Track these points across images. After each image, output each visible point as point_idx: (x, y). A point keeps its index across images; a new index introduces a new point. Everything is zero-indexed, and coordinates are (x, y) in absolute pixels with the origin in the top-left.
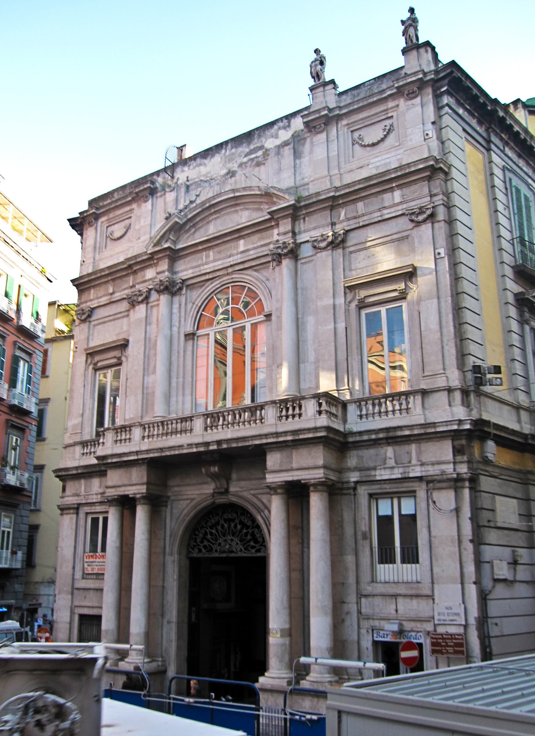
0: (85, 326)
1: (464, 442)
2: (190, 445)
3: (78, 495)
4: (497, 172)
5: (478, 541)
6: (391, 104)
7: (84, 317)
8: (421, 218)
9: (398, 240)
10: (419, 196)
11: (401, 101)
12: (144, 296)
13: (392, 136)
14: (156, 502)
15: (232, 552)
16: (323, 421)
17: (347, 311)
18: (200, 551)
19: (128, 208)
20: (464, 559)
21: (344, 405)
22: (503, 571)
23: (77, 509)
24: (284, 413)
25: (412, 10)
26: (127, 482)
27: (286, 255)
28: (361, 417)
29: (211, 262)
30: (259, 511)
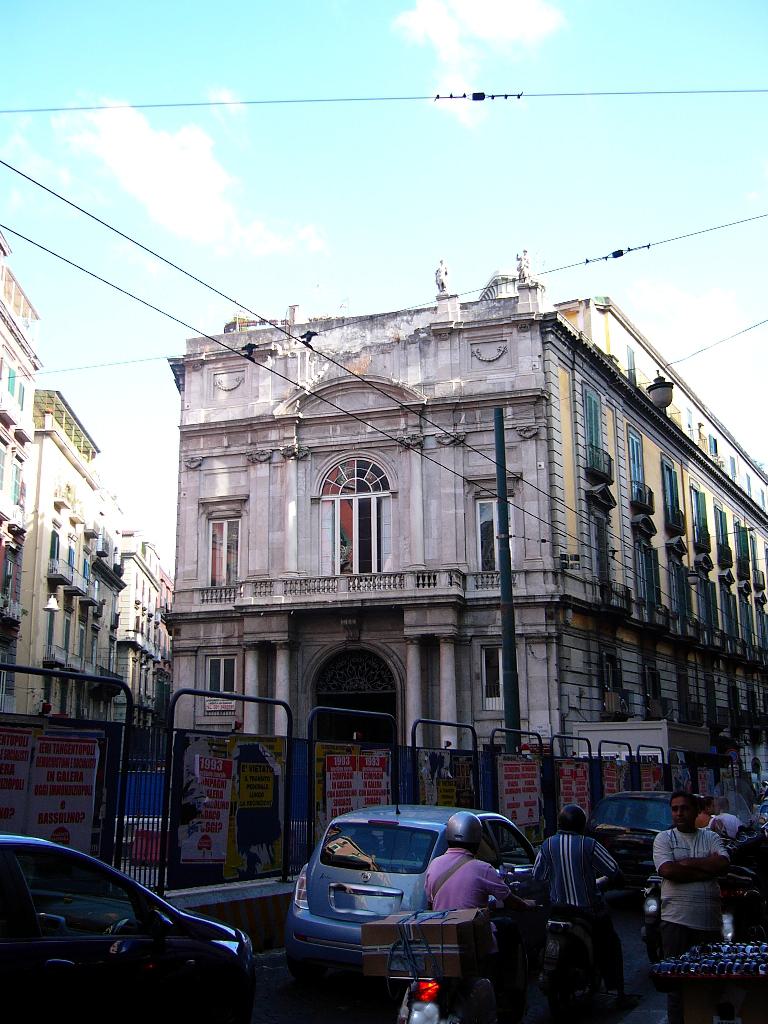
1: (553, 610)
2: (335, 602)
3: (196, 639)
4: (578, 388)
5: (561, 681)
6: (506, 330)
12: (267, 456)
14: (293, 647)
15: (360, 690)
16: (455, 590)
18: (329, 689)
20: (551, 693)
21: (464, 577)
22: (574, 703)
23: (196, 651)
24: (421, 581)
26: (266, 630)
27: (415, 445)
28: (477, 587)
30: (390, 657)
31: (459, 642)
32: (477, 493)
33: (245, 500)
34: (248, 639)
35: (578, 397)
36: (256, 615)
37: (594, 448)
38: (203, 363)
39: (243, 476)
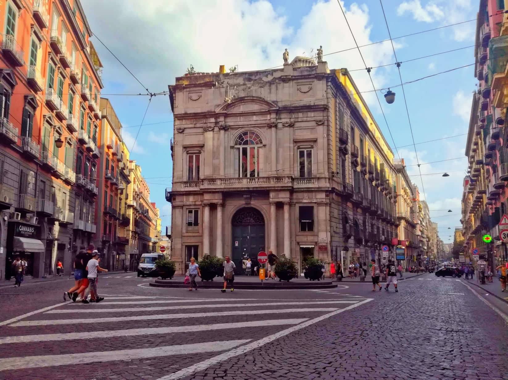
0: (181, 135)
3: (183, 202)
7: (181, 131)
8: (320, 123)
9: (312, 129)
10: (319, 116)
11: (315, 80)
13: (311, 91)
16: (290, 185)
17: (294, 149)
19: (200, 88)
25: (321, 47)
29: (241, 121)
31: (290, 204)
32: (298, 146)
33: (202, 146)
34: (205, 202)
35: (338, 109)
36: (210, 192)
37: (341, 130)
38: (184, 88)
39: (202, 136)
